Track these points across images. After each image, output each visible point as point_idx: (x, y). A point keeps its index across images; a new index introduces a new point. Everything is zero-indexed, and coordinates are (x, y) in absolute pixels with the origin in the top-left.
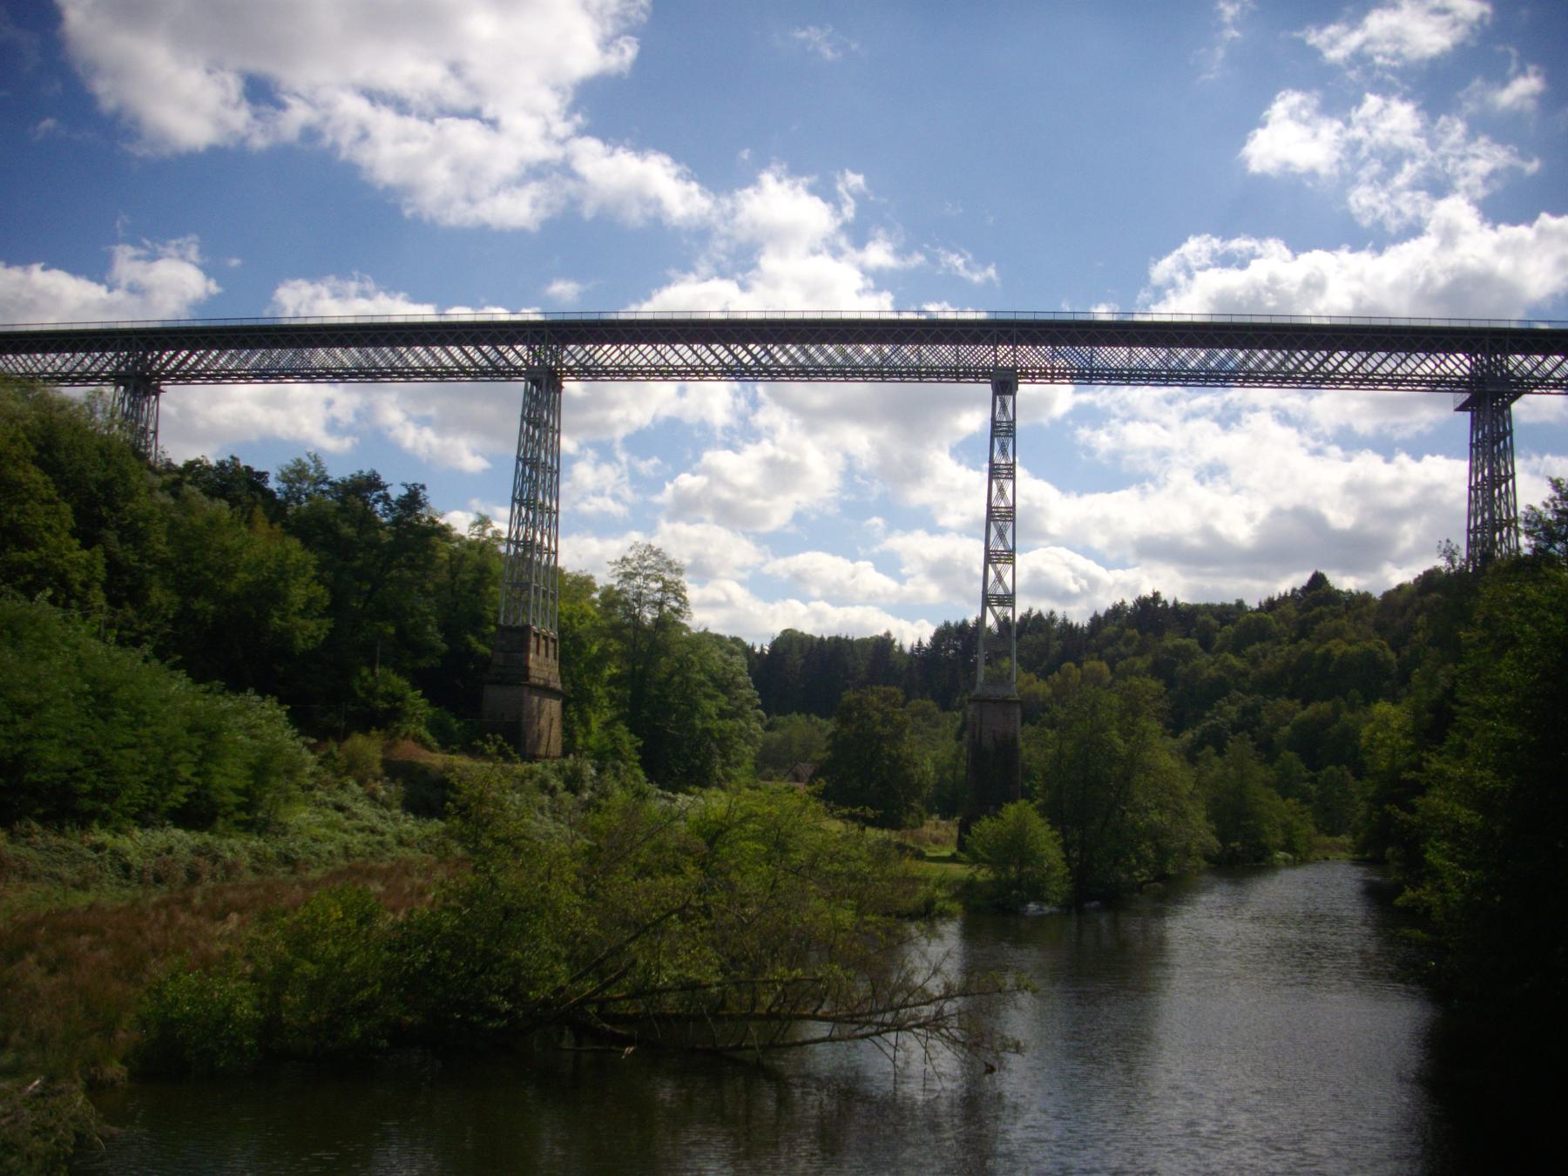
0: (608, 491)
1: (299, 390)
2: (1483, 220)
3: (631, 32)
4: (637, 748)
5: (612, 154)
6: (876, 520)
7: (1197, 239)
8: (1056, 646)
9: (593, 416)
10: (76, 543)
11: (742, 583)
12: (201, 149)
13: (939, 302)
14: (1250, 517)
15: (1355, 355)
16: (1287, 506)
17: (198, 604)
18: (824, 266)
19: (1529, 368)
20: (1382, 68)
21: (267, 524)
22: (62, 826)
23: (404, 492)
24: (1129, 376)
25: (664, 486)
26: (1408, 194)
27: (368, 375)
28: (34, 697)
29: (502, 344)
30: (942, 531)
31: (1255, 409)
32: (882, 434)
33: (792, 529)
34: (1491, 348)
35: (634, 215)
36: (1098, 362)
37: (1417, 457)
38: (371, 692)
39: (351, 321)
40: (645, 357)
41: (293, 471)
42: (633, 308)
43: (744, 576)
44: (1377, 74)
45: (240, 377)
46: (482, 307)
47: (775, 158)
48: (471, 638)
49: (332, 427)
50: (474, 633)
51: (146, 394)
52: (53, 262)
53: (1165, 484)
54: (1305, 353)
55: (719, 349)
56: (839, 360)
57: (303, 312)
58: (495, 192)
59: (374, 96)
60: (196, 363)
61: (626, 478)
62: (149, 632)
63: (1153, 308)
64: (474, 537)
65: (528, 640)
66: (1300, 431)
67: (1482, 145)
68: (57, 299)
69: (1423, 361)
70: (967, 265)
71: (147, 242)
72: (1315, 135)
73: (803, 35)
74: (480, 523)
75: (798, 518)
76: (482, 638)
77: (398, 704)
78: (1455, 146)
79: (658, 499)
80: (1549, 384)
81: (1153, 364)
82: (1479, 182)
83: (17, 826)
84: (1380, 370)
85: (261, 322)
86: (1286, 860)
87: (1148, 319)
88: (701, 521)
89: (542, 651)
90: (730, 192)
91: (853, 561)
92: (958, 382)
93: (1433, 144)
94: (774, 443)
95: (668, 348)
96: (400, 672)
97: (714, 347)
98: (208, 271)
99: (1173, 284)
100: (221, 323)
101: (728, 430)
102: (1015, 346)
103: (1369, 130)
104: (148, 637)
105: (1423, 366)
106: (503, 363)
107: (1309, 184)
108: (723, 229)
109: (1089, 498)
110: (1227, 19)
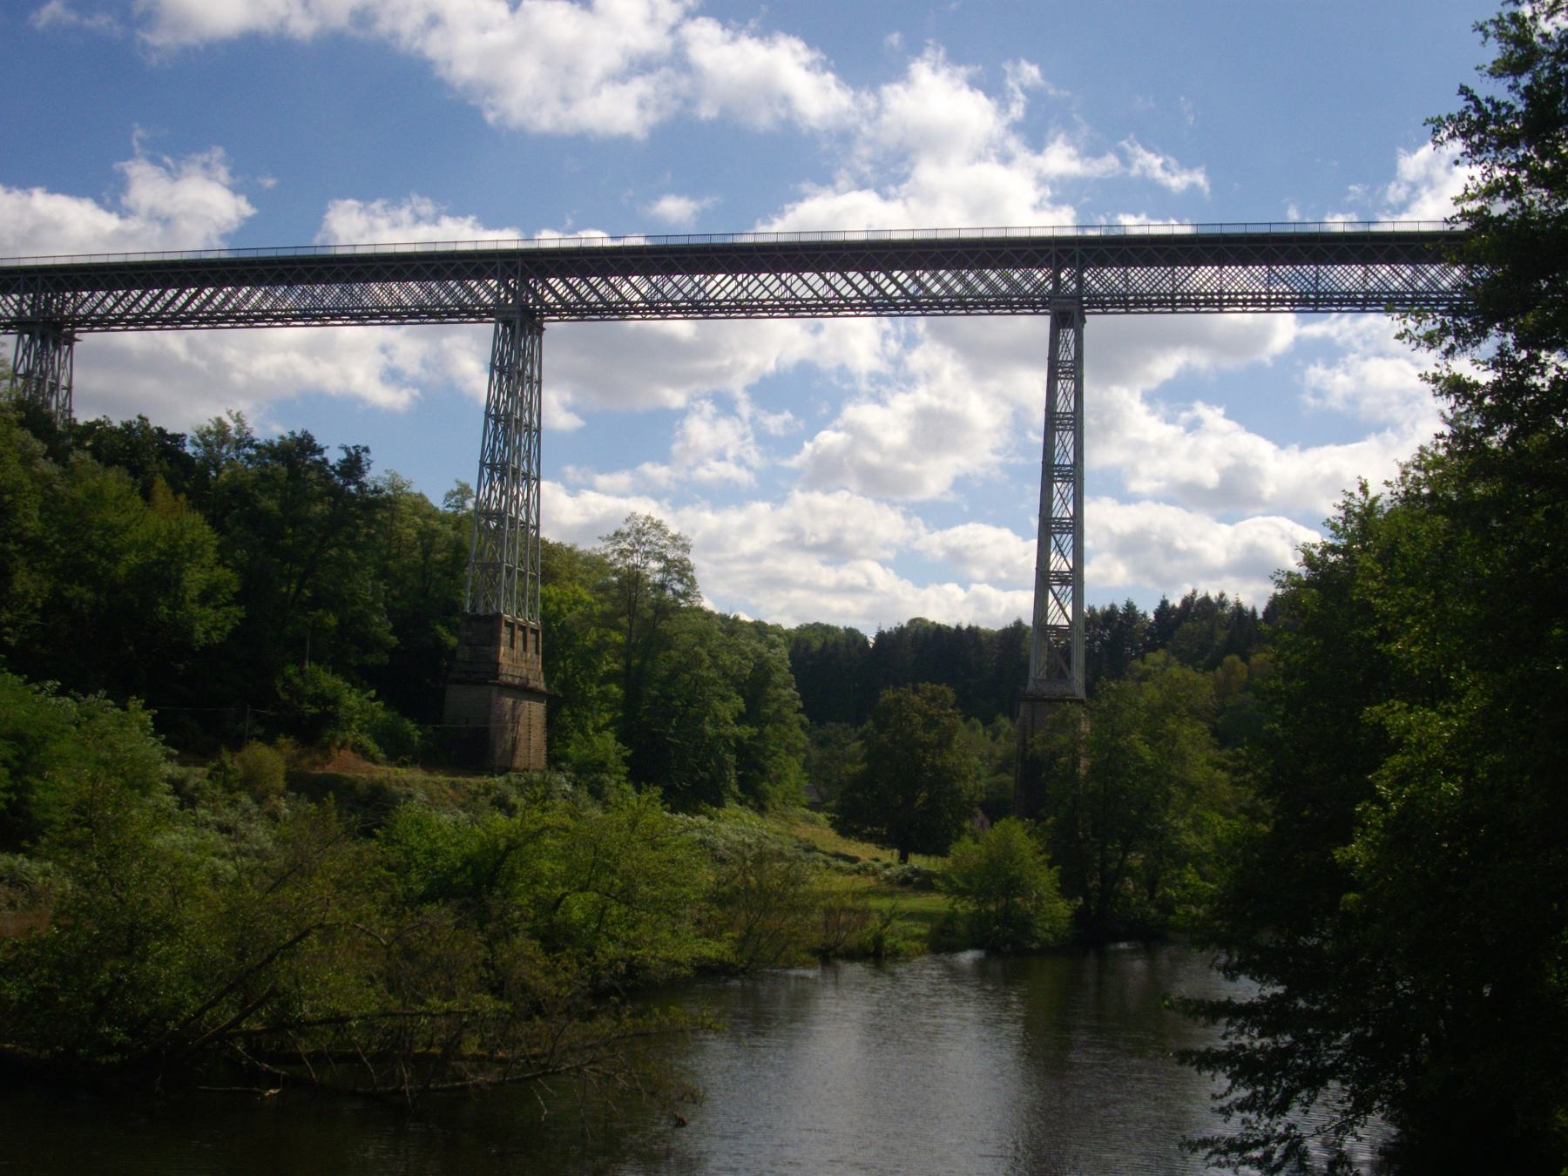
0: (731, 453)
1: (349, 333)
5: (734, 39)
8: (1222, 636)
11: (884, 563)
18: (992, 174)
21: (170, 496)
23: (344, 456)
27: (392, 316)
33: (951, 497)
40: (766, 288)
43: (889, 555)
45: (277, 319)
46: (574, 232)
47: (931, 42)
48: (441, 630)
51: (57, 346)
52: (57, 186)
61: (751, 439)
62: (10, 624)
64: (451, 510)
68: (57, 226)
70: (1164, 167)
71: (167, 160)
74: (459, 492)
75: (960, 483)
76: (454, 629)
77: (330, 708)
81: (1396, 284)
89: (519, 644)
92: (1127, 312)
95: (795, 277)
96: (338, 668)
97: (850, 275)
98: (236, 190)
100: (272, 254)
101: (877, 379)
104: (8, 629)
106: (594, 298)
109: (1313, 454)
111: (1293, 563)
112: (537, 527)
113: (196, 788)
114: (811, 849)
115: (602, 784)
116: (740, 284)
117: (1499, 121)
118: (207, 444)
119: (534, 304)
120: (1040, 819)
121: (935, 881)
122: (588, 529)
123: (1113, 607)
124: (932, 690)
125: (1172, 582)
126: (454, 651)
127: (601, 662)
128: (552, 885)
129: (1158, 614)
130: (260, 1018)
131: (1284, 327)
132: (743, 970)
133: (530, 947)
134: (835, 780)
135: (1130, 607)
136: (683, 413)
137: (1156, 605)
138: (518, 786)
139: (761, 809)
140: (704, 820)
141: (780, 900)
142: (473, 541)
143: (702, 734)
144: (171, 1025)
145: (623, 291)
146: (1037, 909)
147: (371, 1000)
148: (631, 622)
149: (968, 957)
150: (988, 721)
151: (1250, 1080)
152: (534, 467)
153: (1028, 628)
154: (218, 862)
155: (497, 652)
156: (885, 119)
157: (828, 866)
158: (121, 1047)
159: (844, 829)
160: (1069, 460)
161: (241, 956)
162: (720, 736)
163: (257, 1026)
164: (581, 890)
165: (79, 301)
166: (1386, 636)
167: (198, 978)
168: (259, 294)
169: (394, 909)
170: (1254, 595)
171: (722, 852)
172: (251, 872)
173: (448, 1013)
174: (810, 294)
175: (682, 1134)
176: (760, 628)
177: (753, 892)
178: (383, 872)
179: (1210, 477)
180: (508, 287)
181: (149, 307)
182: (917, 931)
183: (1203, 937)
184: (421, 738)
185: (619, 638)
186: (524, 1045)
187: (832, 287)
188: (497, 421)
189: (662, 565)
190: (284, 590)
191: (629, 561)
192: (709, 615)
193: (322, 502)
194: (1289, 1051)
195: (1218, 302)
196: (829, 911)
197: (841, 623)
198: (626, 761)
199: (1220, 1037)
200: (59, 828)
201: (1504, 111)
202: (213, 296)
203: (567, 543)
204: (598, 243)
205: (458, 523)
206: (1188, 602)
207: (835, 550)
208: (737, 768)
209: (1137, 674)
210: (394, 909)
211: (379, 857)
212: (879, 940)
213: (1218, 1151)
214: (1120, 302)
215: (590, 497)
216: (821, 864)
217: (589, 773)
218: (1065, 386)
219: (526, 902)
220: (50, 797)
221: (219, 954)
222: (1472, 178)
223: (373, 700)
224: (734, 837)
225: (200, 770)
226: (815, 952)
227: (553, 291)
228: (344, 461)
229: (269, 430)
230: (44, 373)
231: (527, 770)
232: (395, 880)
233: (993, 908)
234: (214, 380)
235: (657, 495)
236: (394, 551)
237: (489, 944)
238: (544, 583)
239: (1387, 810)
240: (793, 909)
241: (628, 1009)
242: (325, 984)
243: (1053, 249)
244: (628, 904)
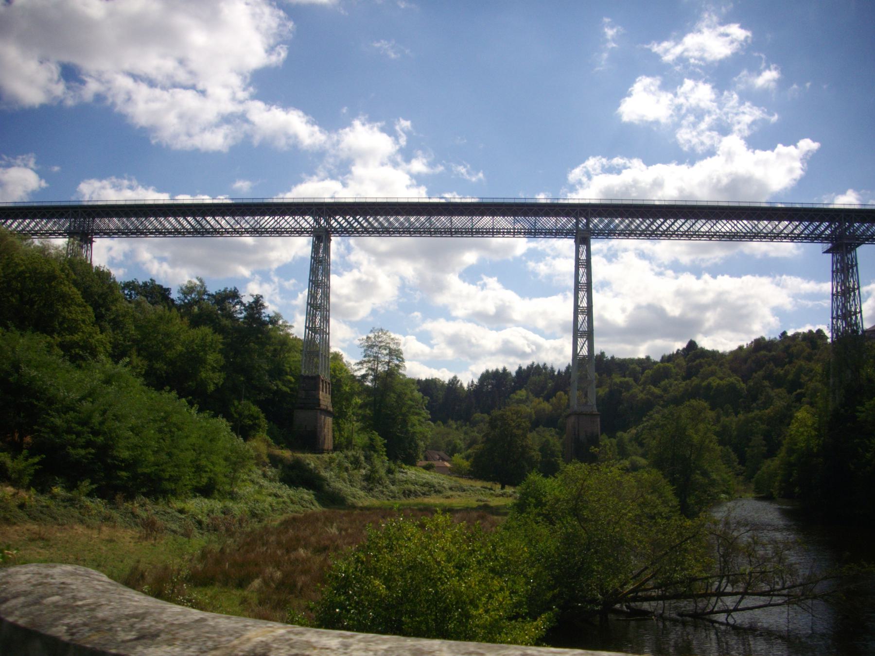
2: (748, 148)
3: (284, 42)
4: (384, 444)
5: (269, 110)
6: (417, 314)
7: (594, 159)
12: (37, 106)
13: (451, 192)
14: (623, 310)
15: (689, 221)
16: (644, 303)
18: (389, 172)
19: (771, 228)
20: (695, 65)
22: (157, 499)
23: (251, 300)
25: (298, 296)
26: (708, 133)
27: (123, 233)
29: (198, 216)
30: (454, 319)
31: (625, 250)
32: (420, 265)
33: (370, 319)
34: (845, 219)
35: (282, 143)
36: (539, 225)
37: (714, 276)
38: (240, 415)
39: (123, 203)
40: (288, 223)
41: (186, 287)
42: (281, 196)
44: (691, 68)
45: (60, 234)
54: (641, 220)
57: (95, 197)
58: (203, 130)
59: (136, 77)
61: (277, 291)
65: (319, 384)
66: (650, 263)
67: (747, 107)
69: (715, 224)
70: (468, 172)
72: (658, 101)
73: (377, 45)
78: (733, 107)
79: (294, 302)
80: (782, 237)
82: (746, 127)
84: (681, 229)
85: (71, 204)
86: (726, 499)
87: (566, 202)
90: (336, 131)
91: (405, 336)
92: (452, 237)
93: (721, 106)
94: (360, 271)
95: (301, 218)
98: (41, 174)
102: (493, 217)
103: (687, 98)
105: (715, 227)
107: (655, 129)
108: (332, 152)
109: (535, 301)
110: (609, 37)
116: (276, 221)
131: (521, 245)
135: (505, 370)
137: (516, 368)
145: (222, 223)
179: (491, 310)
181: (16, 228)
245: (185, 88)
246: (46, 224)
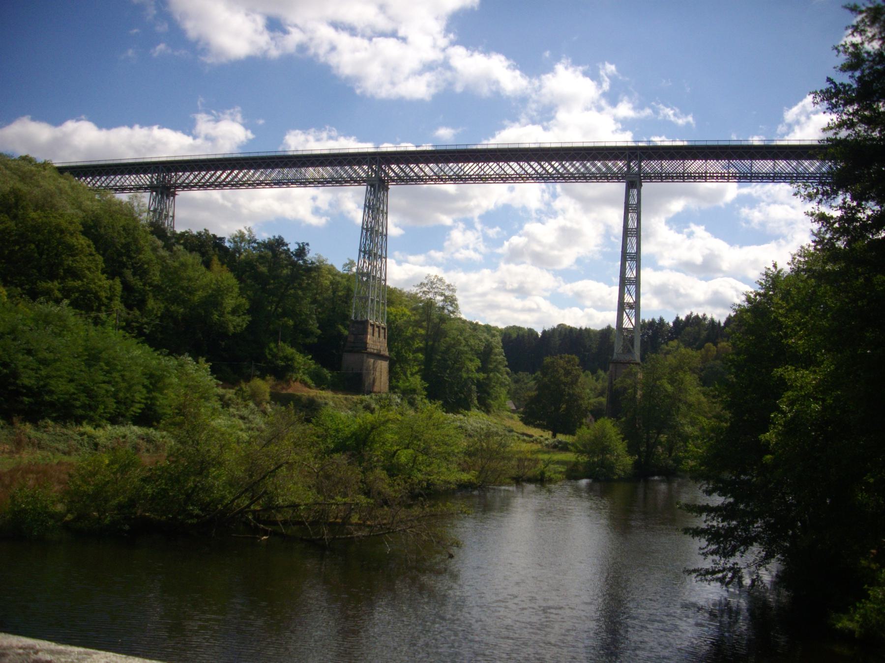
0: (471, 246)
1: (296, 191)
5: (471, 55)
8: (704, 333)
9: (461, 204)
10: (104, 277)
11: (545, 298)
13: (660, 136)
17: (173, 308)
18: (593, 116)
22: (65, 423)
23: (297, 247)
24: (774, 177)
27: (337, 182)
28: (49, 356)
29: (402, 164)
33: (575, 268)
35: (485, 91)
38: (275, 356)
40: (493, 170)
42: (485, 142)
43: (547, 294)
45: (267, 184)
46: (399, 144)
48: (340, 327)
49: (316, 211)
50: (343, 324)
52: (164, 124)
53: (792, 240)
55: (535, 164)
56: (604, 170)
58: (407, 79)
59: (337, 25)
60: (243, 177)
61: (481, 239)
62: (147, 323)
63: (787, 138)
64: (345, 272)
65: (367, 328)
68: (165, 144)
70: (675, 115)
71: (214, 112)
75: (579, 261)
76: (346, 327)
77: (289, 363)
79: (500, 251)
81: (812, 169)
83: (41, 423)
85: (278, 154)
88: (524, 263)
89: (376, 334)
90: (538, 76)
91: (610, 286)
92: (662, 182)
94: (565, 219)
95: (506, 164)
97: (532, 163)
98: (246, 126)
99: (798, 122)
101: (539, 211)
102: (706, 161)
104: (145, 326)
108: (534, 96)
109: (747, 249)
111: (740, 300)
112: (385, 280)
113: (230, 399)
114: (511, 431)
115: (414, 399)
116: (480, 167)
117: (845, 92)
118: (235, 242)
119: (384, 177)
120: (618, 418)
121: (569, 447)
122: (408, 282)
123: (653, 320)
124: (568, 358)
125: (681, 308)
126: (347, 337)
127: (414, 343)
128: (392, 446)
129: (674, 323)
130: (259, 504)
131: (732, 190)
132: (480, 486)
133: (383, 474)
134: (522, 399)
135: (661, 320)
136: (450, 228)
137: (674, 319)
138: (375, 400)
139: (488, 412)
140: (461, 417)
141: (497, 454)
142: (355, 287)
143: (461, 377)
144: (220, 507)
146: (616, 460)
147: (310, 497)
148: (428, 324)
149: (584, 482)
150: (594, 372)
151: (717, 541)
152: (384, 252)
153: (613, 329)
154: (240, 433)
155: (367, 337)
156: (544, 91)
157: (519, 439)
158: (197, 516)
159: (526, 421)
160: (634, 250)
161: (251, 476)
162: (469, 378)
163: (258, 508)
164: (405, 448)
165: (178, 177)
166: (786, 336)
167: (231, 485)
168: (259, 173)
169: (320, 456)
170: (720, 315)
171: (470, 431)
172: (256, 438)
173: (345, 504)
174: (513, 172)
175: (453, 561)
176: (488, 328)
177: (484, 450)
178: (315, 438)
179: (699, 259)
180: (372, 169)
181: (209, 179)
182: (560, 469)
183: (697, 476)
184: (331, 377)
185: (422, 331)
186: (380, 519)
187: (523, 169)
188: (367, 230)
189: (443, 298)
190: (270, 308)
191: (428, 296)
192: (464, 322)
193: (287, 268)
194: (736, 528)
195: (703, 177)
196: (520, 460)
197: (526, 326)
198: (426, 389)
199: (702, 522)
200: (169, 416)
201: (847, 88)
202: (238, 174)
203: (399, 288)
204: (389, 150)
205: (349, 278)
206: (688, 318)
207: (521, 292)
208: (477, 392)
209: (664, 351)
210: (320, 456)
211: (313, 432)
212: (543, 473)
213: (701, 574)
214: (658, 176)
215: (406, 266)
216: (516, 438)
217: (408, 394)
218: (632, 216)
219: (380, 453)
220: (165, 402)
221: (242, 475)
222: (832, 120)
223: (310, 360)
224: (475, 424)
225: (231, 391)
226: (513, 479)
227: (393, 171)
228: (297, 250)
229: (263, 236)
230: (162, 210)
231: (380, 392)
232: (320, 442)
233: (596, 460)
234: (235, 214)
235: (437, 265)
236: (319, 291)
237: (363, 472)
238: (388, 306)
239: (785, 417)
240: (503, 458)
241: (428, 503)
242: (289, 489)
243: (627, 152)
244: (427, 455)
245: (384, 35)
246: (254, 174)
